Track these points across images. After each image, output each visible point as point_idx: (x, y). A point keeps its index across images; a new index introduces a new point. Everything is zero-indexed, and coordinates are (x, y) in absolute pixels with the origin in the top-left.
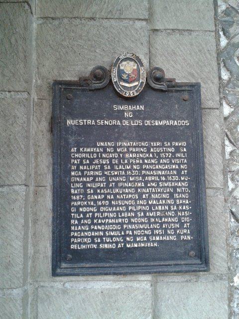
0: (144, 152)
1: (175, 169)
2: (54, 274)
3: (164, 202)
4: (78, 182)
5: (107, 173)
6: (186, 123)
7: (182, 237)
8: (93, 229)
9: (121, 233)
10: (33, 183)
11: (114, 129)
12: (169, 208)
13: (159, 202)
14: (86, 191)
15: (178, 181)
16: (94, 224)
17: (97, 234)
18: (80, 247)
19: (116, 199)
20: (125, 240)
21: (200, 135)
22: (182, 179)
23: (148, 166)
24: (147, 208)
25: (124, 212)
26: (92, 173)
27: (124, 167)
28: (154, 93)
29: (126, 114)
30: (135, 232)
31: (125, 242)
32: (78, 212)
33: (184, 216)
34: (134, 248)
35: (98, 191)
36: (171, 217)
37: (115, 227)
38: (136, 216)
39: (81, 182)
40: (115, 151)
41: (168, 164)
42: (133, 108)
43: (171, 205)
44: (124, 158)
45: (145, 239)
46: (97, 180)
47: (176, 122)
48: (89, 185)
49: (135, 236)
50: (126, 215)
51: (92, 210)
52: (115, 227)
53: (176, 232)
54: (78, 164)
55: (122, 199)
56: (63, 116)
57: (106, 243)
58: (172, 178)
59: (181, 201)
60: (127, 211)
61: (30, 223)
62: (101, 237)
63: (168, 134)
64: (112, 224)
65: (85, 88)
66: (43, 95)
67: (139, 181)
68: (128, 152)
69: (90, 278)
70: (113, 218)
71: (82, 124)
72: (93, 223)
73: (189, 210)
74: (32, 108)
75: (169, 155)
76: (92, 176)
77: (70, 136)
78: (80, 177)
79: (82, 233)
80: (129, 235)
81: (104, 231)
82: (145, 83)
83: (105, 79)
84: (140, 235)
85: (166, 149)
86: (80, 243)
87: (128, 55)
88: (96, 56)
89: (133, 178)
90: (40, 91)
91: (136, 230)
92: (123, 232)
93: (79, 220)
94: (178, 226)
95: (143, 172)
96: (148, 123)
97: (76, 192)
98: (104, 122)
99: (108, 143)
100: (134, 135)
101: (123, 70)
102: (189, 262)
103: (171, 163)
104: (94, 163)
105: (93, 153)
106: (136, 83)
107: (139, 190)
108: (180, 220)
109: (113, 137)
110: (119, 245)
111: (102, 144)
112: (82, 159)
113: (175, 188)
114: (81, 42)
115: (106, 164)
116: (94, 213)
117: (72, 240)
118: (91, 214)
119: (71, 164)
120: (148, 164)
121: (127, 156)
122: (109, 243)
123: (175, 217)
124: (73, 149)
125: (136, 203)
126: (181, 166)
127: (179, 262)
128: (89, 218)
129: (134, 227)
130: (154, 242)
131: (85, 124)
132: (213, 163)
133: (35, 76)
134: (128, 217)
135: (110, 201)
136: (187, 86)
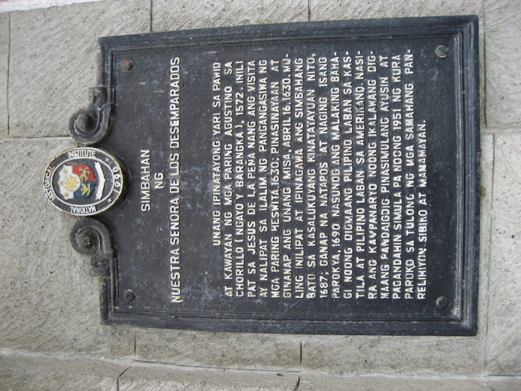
0: (233, 150)
1: (268, 85)
2: (472, 331)
3: (334, 109)
4: (293, 285)
5: (275, 227)
6: (175, 63)
7: (408, 72)
9: (397, 199)
10: (296, 369)
12: (347, 97)
13: (335, 119)
16: (379, 252)
17: (397, 248)
23: (261, 142)
26: (274, 257)
27: (263, 191)
33: (365, 66)
34: (428, 170)
35: (311, 244)
36: (366, 94)
37: (385, 210)
38: (364, 167)
41: (257, 100)
42: (145, 172)
43: (341, 93)
45: (410, 148)
46: (288, 247)
47: (172, 85)
48: (299, 263)
49: (405, 169)
50: (360, 188)
51: (351, 256)
52: (385, 210)
54: (256, 284)
60: (353, 184)
61: (371, 375)
62: (405, 239)
63: (198, 101)
64: (379, 216)
68: (233, 181)
69: (483, 260)
70: (367, 214)
74: (153, 365)
76: (281, 257)
77: (203, 299)
78: (282, 282)
79: (395, 277)
80: (403, 183)
81: (392, 232)
84: (403, 158)
86: (416, 281)
87: (48, 183)
88: (54, 242)
89: (286, 172)
91: (391, 168)
92: (396, 195)
93: (369, 283)
94: (384, 80)
97: (312, 289)
98: (173, 231)
100: (199, 170)
101: (75, 194)
102: (457, 61)
103: (255, 94)
104: (254, 253)
105: (234, 254)
107: (311, 160)
108: (373, 76)
110: (421, 202)
111: (216, 235)
112: (246, 276)
113: (306, 85)
114: (31, 269)
115: (257, 228)
116: (355, 254)
118: (358, 260)
120: (257, 139)
122: (416, 223)
123: (365, 86)
124: (227, 294)
125: (336, 166)
130: (416, 132)
131: (178, 268)
132: (259, 6)
133: (94, 355)
134: (366, 182)
135: (331, 220)
136: (103, 65)
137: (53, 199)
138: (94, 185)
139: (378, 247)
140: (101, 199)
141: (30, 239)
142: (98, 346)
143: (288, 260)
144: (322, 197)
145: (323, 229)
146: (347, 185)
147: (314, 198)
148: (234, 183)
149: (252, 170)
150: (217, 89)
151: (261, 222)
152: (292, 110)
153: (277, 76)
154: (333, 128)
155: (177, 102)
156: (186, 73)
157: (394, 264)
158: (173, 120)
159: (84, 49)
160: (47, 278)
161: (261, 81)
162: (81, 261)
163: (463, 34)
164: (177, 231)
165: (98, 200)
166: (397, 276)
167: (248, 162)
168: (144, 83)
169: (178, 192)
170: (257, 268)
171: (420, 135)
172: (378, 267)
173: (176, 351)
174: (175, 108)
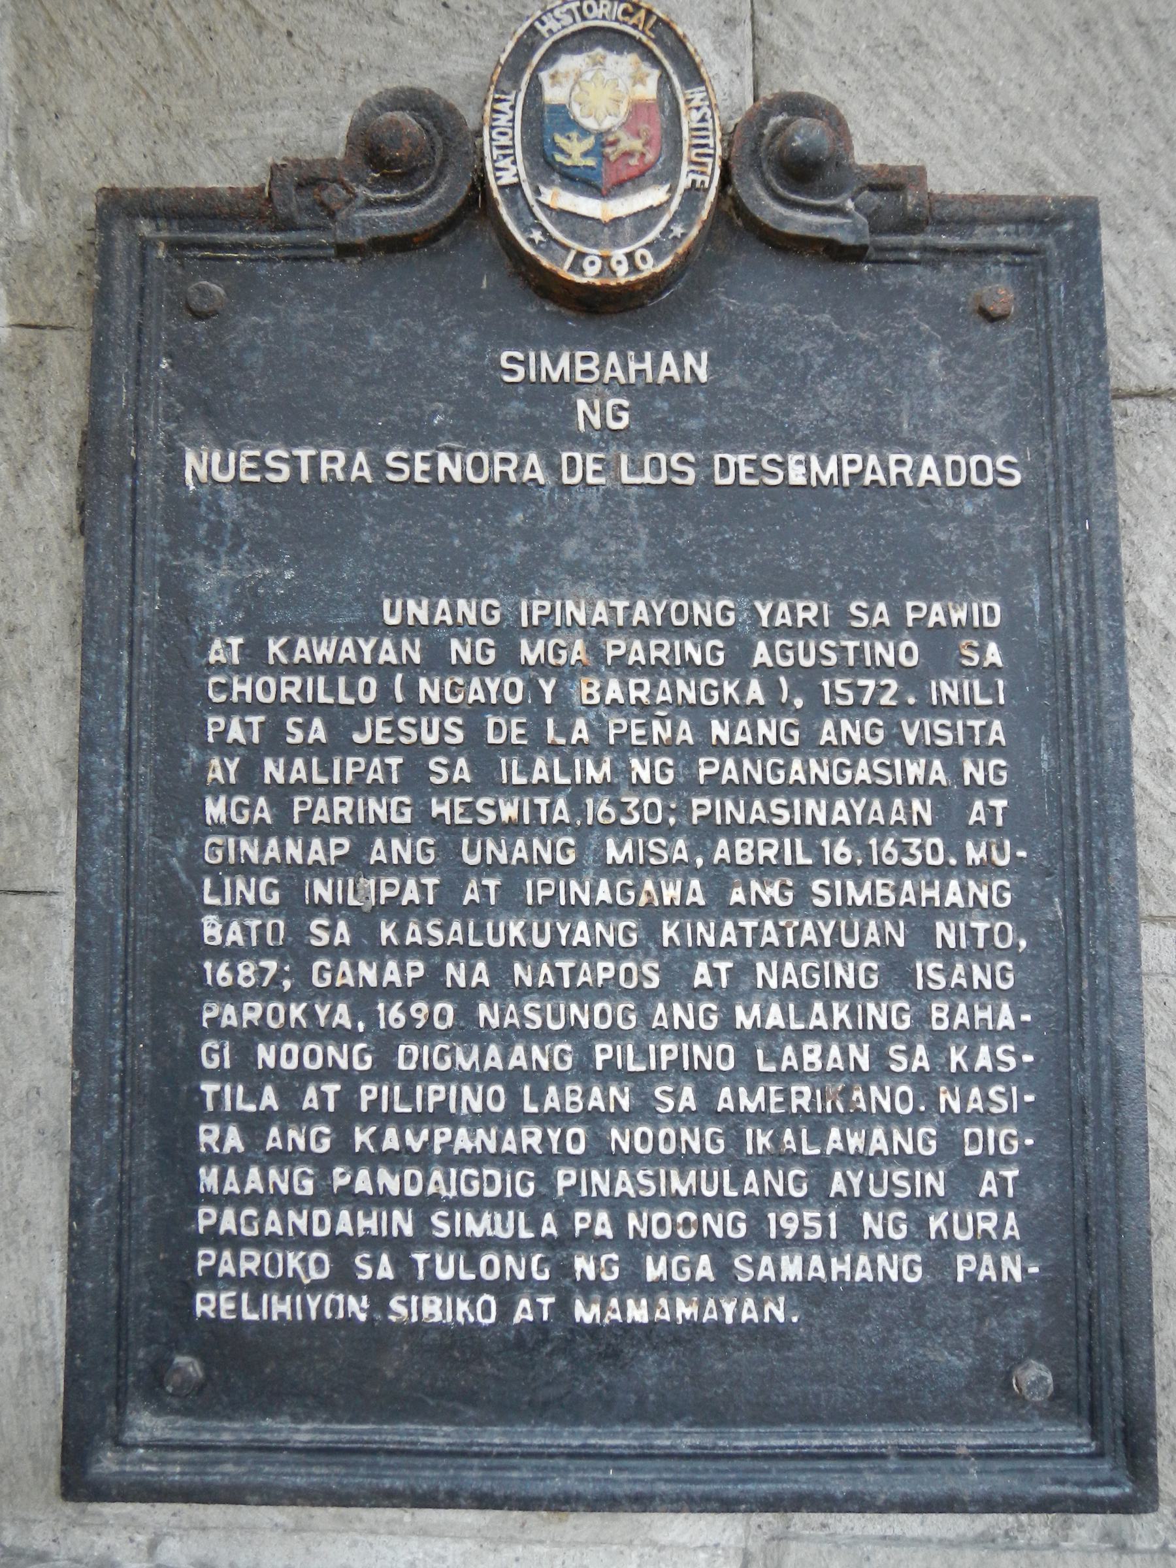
3: (840, 1013)
4: (246, 869)
5: (445, 809)
6: (1004, 467)
7: (964, 1263)
8: (347, 1190)
9: (534, 1223)
11: (500, 513)
12: (880, 1056)
13: (804, 1012)
14: (299, 932)
15: (944, 872)
18: (255, 1305)
19: (504, 988)
20: (563, 1270)
21: (1100, 549)
22: (974, 855)
23: (730, 763)
24: (723, 1056)
25: (560, 1078)
27: (567, 769)
28: (779, 266)
29: (582, 405)
30: (632, 1220)
31: (566, 1286)
32: (246, 1072)
33: (983, 1118)
35: (387, 932)
36: (890, 1119)
38: (645, 1110)
39: (273, 868)
40: (508, 661)
42: (633, 366)
44: (565, 711)
45: (705, 1268)
48: (322, 890)
49: (634, 1250)
50: (572, 1099)
53: (924, 1224)
54: (250, 745)
55: (546, 992)
56: (158, 429)
57: (434, 1286)
58: (904, 849)
59: (962, 1008)
60: (584, 1071)
62: (400, 1248)
63: (883, 546)
64: (478, 1159)
65: (307, 235)
66: (47, 298)
67: (669, 870)
68: (597, 663)
70: (484, 1119)
71: (285, 476)
72: (343, 1152)
73: (1020, 1077)
75: (881, 689)
76: (341, 828)
77: (200, 561)
78: (261, 831)
79: (273, 1215)
80: (590, 1242)
81: (424, 1206)
82: (712, 195)
83: (441, 174)
84: (672, 1245)
85: (859, 650)
86: (256, 1285)
89: (628, 848)
90: (32, 271)
91: (640, 1203)
92: (548, 1217)
93: (254, 1126)
94: (935, 1182)
95: (701, 806)
96: (737, 466)
97: (235, 935)
98: (432, 460)
99: (462, 604)
100: (637, 556)
101: (561, 110)
103: (895, 745)
104: (358, 738)
105: (354, 670)
106: (654, 196)
107: (668, 932)
108: (950, 1144)
109: (493, 562)
110: (525, 1303)
111: (418, 611)
112: (277, 711)
113: (921, 919)
115: (441, 747)
116: (350, 1080)
117: (205, 1258)
118: (331, 1088)
119: (204, 746)
121: (587, 690)
122: (454, 1287)
123: (918, 1118)
124: (217, 644)
125: (646, 1018)
126: (968, 767)
127: (935, 1436)
128: (321, 1114)
129: (624, 1184)
130: (761, 1289)
131: (305, 476)
134: (590, 1117)
135: (467, 999)
137: (544, 30)
139: (377, 1159)
140: (543, 205)
142: (36, 197)
144: (545, 969)
148: (597, 673)
151: (462, 762)
153: (952, 822)
155: (868, 478)
159: (1044, 160)
160: (270, 18)
162: (326, 136)
165: (537, 192)
166: (273, 1224)
167: (662, 719)
168: (934, 363)
170: (306, 750)
171: (750, 1303)
172: (307, 1156)
173: (24, 468)
174: (847, 470)
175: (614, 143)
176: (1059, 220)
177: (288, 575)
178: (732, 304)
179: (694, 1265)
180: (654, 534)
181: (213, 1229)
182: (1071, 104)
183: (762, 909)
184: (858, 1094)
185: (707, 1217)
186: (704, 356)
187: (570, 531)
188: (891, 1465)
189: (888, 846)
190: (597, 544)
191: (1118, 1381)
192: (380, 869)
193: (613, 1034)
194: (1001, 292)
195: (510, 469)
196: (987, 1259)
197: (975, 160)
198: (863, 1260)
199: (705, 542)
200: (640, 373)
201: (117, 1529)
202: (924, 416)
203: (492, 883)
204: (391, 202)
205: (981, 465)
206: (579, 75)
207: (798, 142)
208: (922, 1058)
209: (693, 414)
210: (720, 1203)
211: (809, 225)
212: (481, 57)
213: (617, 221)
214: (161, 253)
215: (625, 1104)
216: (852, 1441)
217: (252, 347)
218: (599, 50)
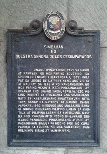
0: (62, 75)
2: (9, 145)
3: (74, 106)
4: (22, 93)
6: (90, 57)
7: (84, 127)
9: (47, 123)
12: (77, 109)
13: (71, 105)
14: (27, 98)
16: (32, 118)
17: (33, 123)
18: (23, 130)
19: (45, 103)
21: (98, 64)
22: (86, 92)
23: (64, 84)
24: (64, 109)
26: (30, 88)
27: (50, 84)
28: (70, 37)
29: (52, 51)
30: (56, 123)
31: (50, 129)
32: (22, 110)
33: (86, 115)
35: (34, 98)
36: (78, 115)
37: (44, 120)
38: (57, 114)
39: (24, 93)
40: (45, 74)
42: (56, 47)
44: (50, 79)
45: (62, 127)
46: (34, 92)
47: (83, 56)
48: (29, 95)
49: (56, 125)
51: (31, 110)
52: (44, 120)
53: (81, 124)
54: (22, 82)
55: (48, 104)
56: (13, 53)
57: (39, 129)
58: (79, 91)
59: (84, 105)
60: (52, 110)
62: (36, 125)
63: (78, 64)
64: (43, 118)
65: (27, 34)
67: (59, 93)
68: (53, 75)
69: (29, 148)
70: (43, 114)
71: (25, 57)
72: (31, 117)
75: (78, 77)
76: (30, 89)
77: (17, 65)
78: (23, 90)
79: (25, 123)
80: (52, 125)
81: (38, 122)
84: (59, 125)
85: (76, 74)
86: (23, 129)
88: (34, 13)
89: (55, 91)
91: (56, 122)
92: (48, 123)
93: (23, 115)
95: (62, 87)
96: (65, 57)
97: (21, 99)
98: (38, 56)
99: (41, 69)
100: (56, 65)
101: (50, 22)
103: (79, 82)
105: (31, 75)
107: (59, 98)
108: (83, 117)
110: (46, 130)
111: (37, 70)
112: (25, 79)
113: (81, 97)
115: (39, 82)
116: (31, 111)
118: (30, 112)
119: (18, 82)
120: (65, 83)
121: (52, 77)
122: (40, 129)
123: (80, 115)
124: (19, 73)
125: (57, 106)
126: (85, 84)
127: (81, 141)
128: (29, 114)
129: (55, 120)
130: (67, 129)
131: (27, 57)
134: (52, 114)
135: (41, 104)
138: (52, 30)
139: (34, 118)
140: (49, 32)
141: (35, 4)
143: (30, 92)
144: (48, 102)
145: (39, 102)
146: (52, 109)
147: (48, 99)
148: (53, 75)
149: (56, 81)
150: (81, 70)
151: (41, 84)
152: (73, 93)
153: (84, 89)
154: (68, 105)
155: (77, 58)
156: (87, 60)
157: (29, 123)
158: (72, 56)
159: (96, 23)
160: (21, 10)
161: (83, 84)
163: (94, 143)
164: (38, 57)
165: (48, 31)
166: (25, 124)
168: (84, 47)
169: (50, 58)
170: (27, 82)
171: (66, 130)
172: (28, 118)
175: (55, 26)
176: (96, 32)
177: (25, 66)
178: (65, 41)
179: (61, 127)
180: (58, 63)
181: (20, 124)
182: (99, 17)
183: (67, 97)
184: (75, 112)
185: (62, 123)
186: (63, 46)
187: (51, 62)
188: (77, 143)
189: (78, 91)
190: (53, 64)
191: (97, 137)
192: (34, 93)
193: (54, 107)
194: (91, 39)
195: (45, 57)
196: (86, 126)
197: (89, 23)
198: (75, 126)
199: (63, 64)
200: (57, 48)
201: (11, 150)
202: (83, 52)
203: (44, 94)
204: (34, 31)
205: (88, 56)
206: (52, 19)
207: (72, 26)
208: (81, 109)
209: (62, 52)
210: (63, 122)
211: (73, 33)
212: (42, 15)
213: (55, 34)
214: (13, 35)
215: (55, 113)
216: (74, 142)
217: (21, 45)
218: (54, 16)
